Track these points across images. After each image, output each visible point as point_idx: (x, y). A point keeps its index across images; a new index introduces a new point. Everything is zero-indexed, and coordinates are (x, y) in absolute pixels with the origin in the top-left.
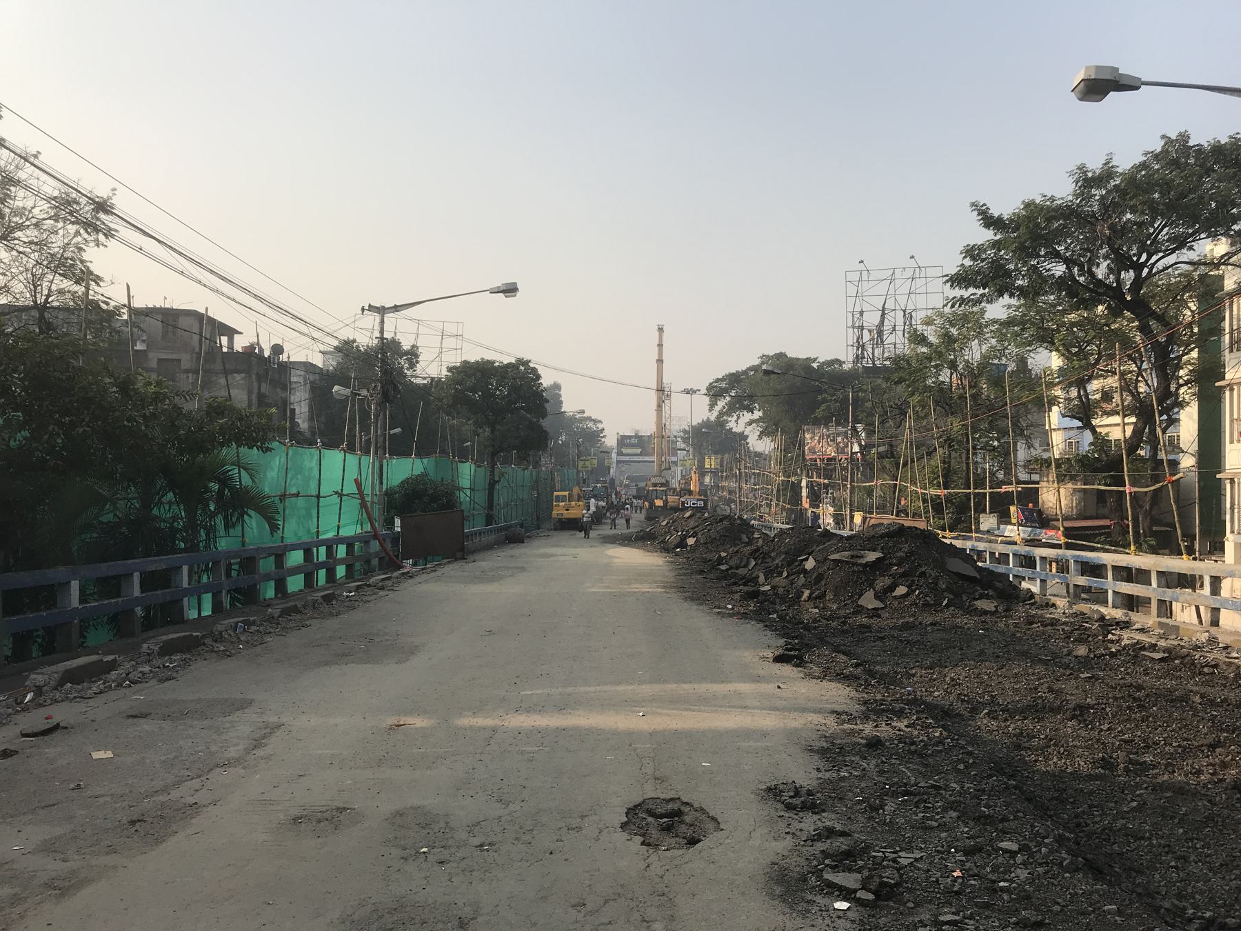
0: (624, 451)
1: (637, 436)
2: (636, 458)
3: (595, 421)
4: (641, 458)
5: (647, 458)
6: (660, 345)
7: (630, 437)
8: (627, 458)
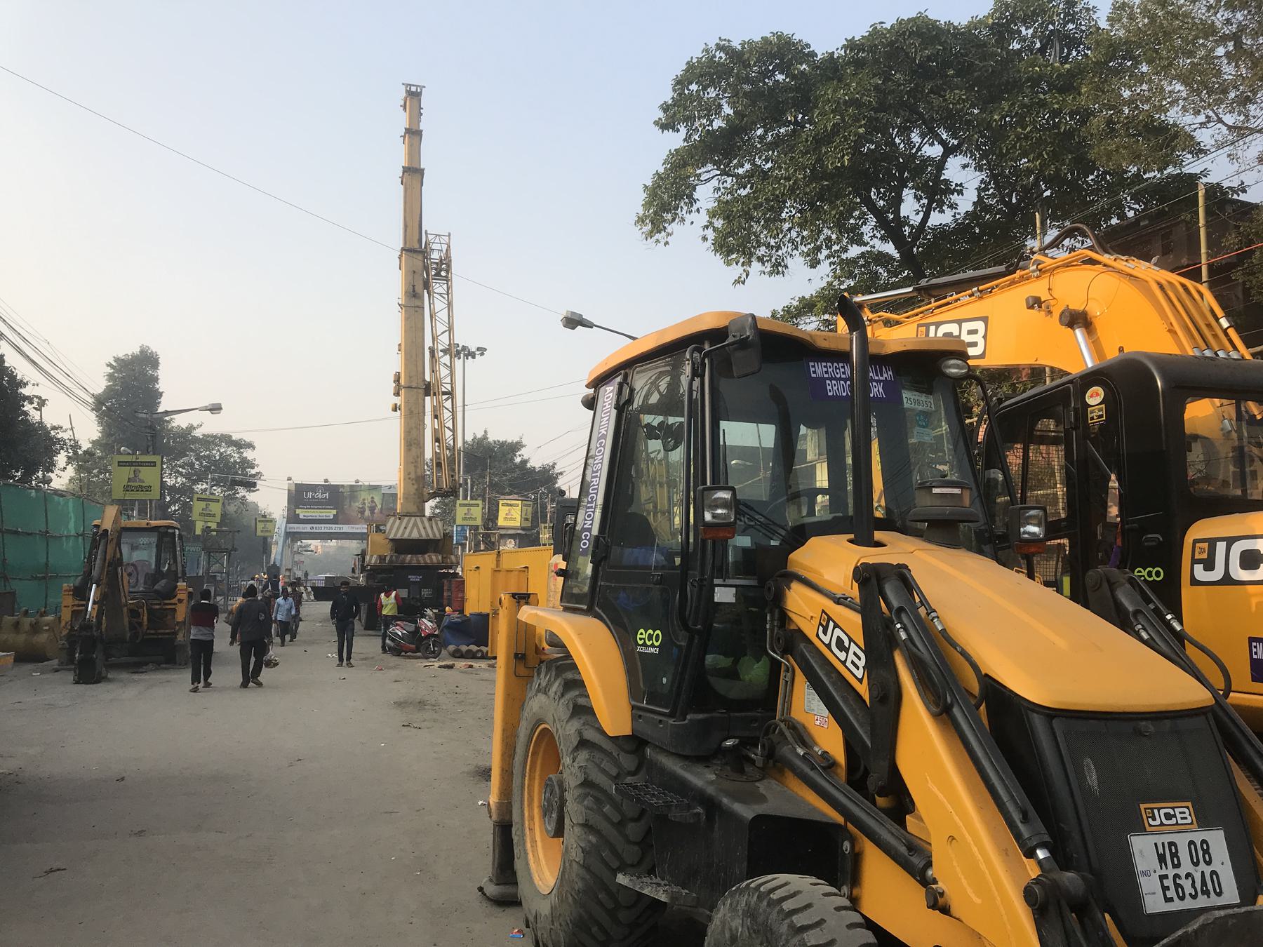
0: (302, 513)
1: (328, 487)
2: (324, 528)
3: (240, 445)
4: (334, 528)
5: (346, 528)
6: (413, 173)
7: (313, 488)
8: (307, 528)
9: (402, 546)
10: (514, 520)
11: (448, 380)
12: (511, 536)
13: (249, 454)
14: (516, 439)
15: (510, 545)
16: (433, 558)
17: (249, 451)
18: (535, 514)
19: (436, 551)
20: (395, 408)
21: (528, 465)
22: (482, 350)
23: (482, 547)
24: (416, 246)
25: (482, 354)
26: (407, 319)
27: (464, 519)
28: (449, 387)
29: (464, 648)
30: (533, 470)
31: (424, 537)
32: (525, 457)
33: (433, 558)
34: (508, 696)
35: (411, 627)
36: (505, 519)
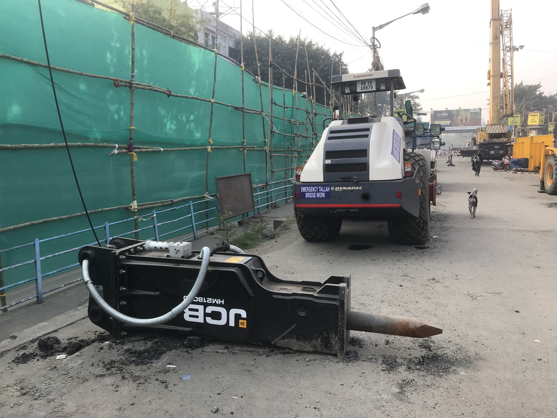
5: (455, 128)
7: (441, 112)
9: (492, 136)
10: (536, 122)
11: (510, 71)
12: (534, 129)
13: (417, 101)
14: (537, 84)
15: (533, 134)
16: (504, 140)
17: (417, 99)
18: (546, 118)
19: (505, 137)
20: (489, 84)
21: (543, 95)
22: (522, 47)
23: (521, 134)
24: (497, 17)
25: (522, 48)
26: (493, 48)
27: (512, 123)
28: (510, 74)
29: (519, 169)
30: (545, 97)
31: (501, 132)
32: (542, 92)
33: (504, 140)
34: (544, 162)
35: (501, 162)
36: (531, 122)
